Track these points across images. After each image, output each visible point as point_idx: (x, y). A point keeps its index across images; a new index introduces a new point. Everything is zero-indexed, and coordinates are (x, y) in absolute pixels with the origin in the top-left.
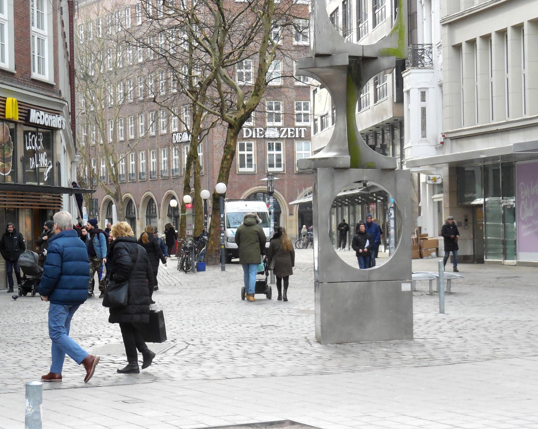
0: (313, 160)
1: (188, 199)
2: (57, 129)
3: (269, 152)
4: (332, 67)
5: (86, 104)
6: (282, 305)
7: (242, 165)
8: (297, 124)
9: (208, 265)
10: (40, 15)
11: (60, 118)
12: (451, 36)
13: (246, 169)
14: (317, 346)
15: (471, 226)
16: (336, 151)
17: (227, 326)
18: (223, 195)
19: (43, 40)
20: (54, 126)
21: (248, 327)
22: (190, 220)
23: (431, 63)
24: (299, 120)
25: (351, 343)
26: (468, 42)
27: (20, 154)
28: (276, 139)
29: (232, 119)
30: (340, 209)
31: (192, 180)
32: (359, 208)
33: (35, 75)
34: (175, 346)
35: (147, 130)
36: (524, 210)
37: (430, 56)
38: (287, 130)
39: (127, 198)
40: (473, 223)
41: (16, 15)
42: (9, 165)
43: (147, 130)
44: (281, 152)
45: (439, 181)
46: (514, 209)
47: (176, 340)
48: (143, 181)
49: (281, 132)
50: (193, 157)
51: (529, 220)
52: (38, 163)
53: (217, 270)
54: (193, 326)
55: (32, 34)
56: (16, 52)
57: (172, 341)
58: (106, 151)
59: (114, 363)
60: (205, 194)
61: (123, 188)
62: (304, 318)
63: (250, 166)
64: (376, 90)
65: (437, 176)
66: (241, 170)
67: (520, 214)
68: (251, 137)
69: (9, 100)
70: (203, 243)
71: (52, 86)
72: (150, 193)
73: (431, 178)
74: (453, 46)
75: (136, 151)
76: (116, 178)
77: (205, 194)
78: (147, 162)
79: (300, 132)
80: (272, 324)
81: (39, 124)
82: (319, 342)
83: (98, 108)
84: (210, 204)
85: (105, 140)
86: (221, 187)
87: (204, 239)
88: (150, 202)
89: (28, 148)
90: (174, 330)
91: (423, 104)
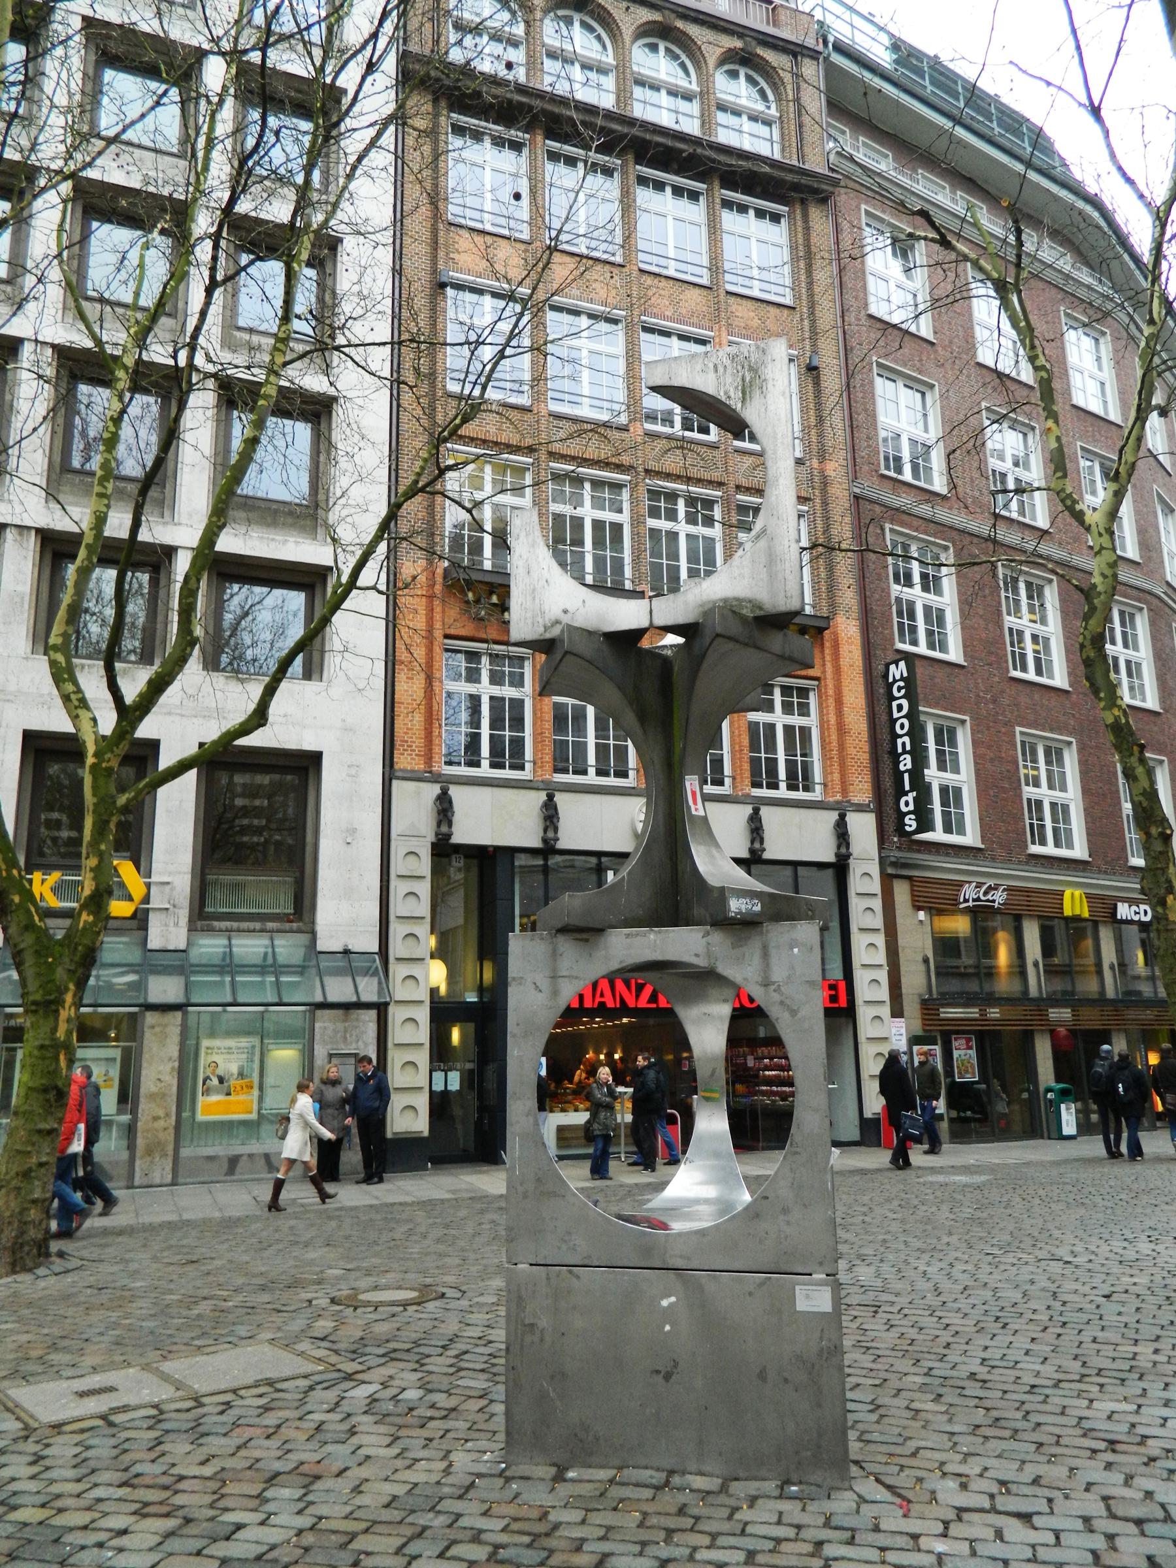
56: (1088, 834)
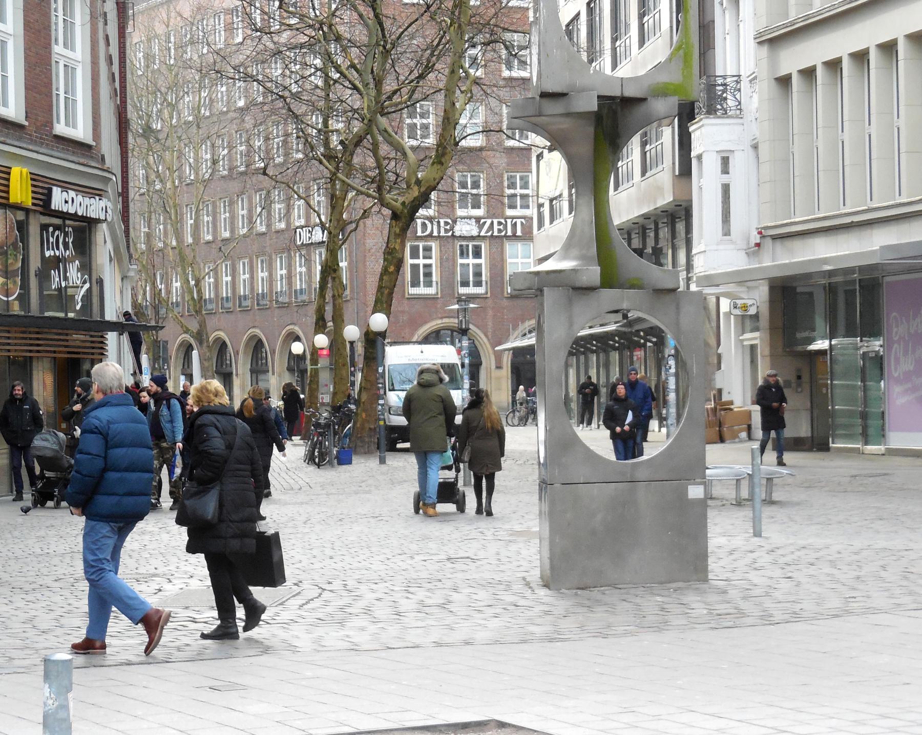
0: (537, 273)
1: (321, 340)
2: (97, 221)
3: (461, 261)
4: (568, 115)
5: (147, 178)
6: (484, 523)
7: (415, 283)
8: (509, 212)
9: (356, 453)
10: (69, 26)
11: (103, 203)
12: (773, 62)
13: (422, 290)
14: (543, 592)
15: (806, 387)
16: (575, 258)
17: (388, 559)
18: (383, 335)
19: (74, 69)
20: (93, 216)
21: (425, 561)
22: (325, 377)
23: (739, 107)
24: (512, 206)
25: (602, 588)
26: (801, 72)
27: (35, 264)
28: (472, 238)
29: (398, 205)
30: (582, 358)
31: (329, 309)
32: (615, 356)
33: (61, 129)
34: (300, 593)
35: (251, 222)
36: (897, 360)
37: (738, 96)
38: (492, 223)
39: (218, 339)
40: (811, 382)
41: (27, 25)
42: (15, 282)
43: (251, 222)
44: (481, 261)
45: (753, 311)
46: (882, 357)
47: (301, 582)
48: (246, 311)
49: (481, 227)
50: (330, 270)
51: (907, 376)
52: (66, 279)
53: (372, 463)
54: (331, 558)
55: (54, 58)
56: (27, 88)
57: (295, 584)
58: (183, 258)
59: (196, 622)
60: (352, 332)
61: (211, 323)
62: (521, 545)
63: (429, 284)
64: (644, 154)
65: (750, 302)
66: (413, 291)
67: (890, 366)
68: (431, 235)
69: (16, 171)
70: (348, 417)
71: (89, 147)
72: (257, 331)
73: (739, 306)
74: (777, 79)
75: (232, 259)
76: (198, 305)
77: (352, 332)
78: (252, 278)
79: (514, 226)
80: (466, 555)
81: (67, 213)
82: (546, 586)
83: (169, 185)
84: (360, 349)
85: (180, 239)
86: (379, 321)
87: (350, 410)
88: (257, 346)
89: (47, 254)
90: (298, 565)
91: (725, 179)
